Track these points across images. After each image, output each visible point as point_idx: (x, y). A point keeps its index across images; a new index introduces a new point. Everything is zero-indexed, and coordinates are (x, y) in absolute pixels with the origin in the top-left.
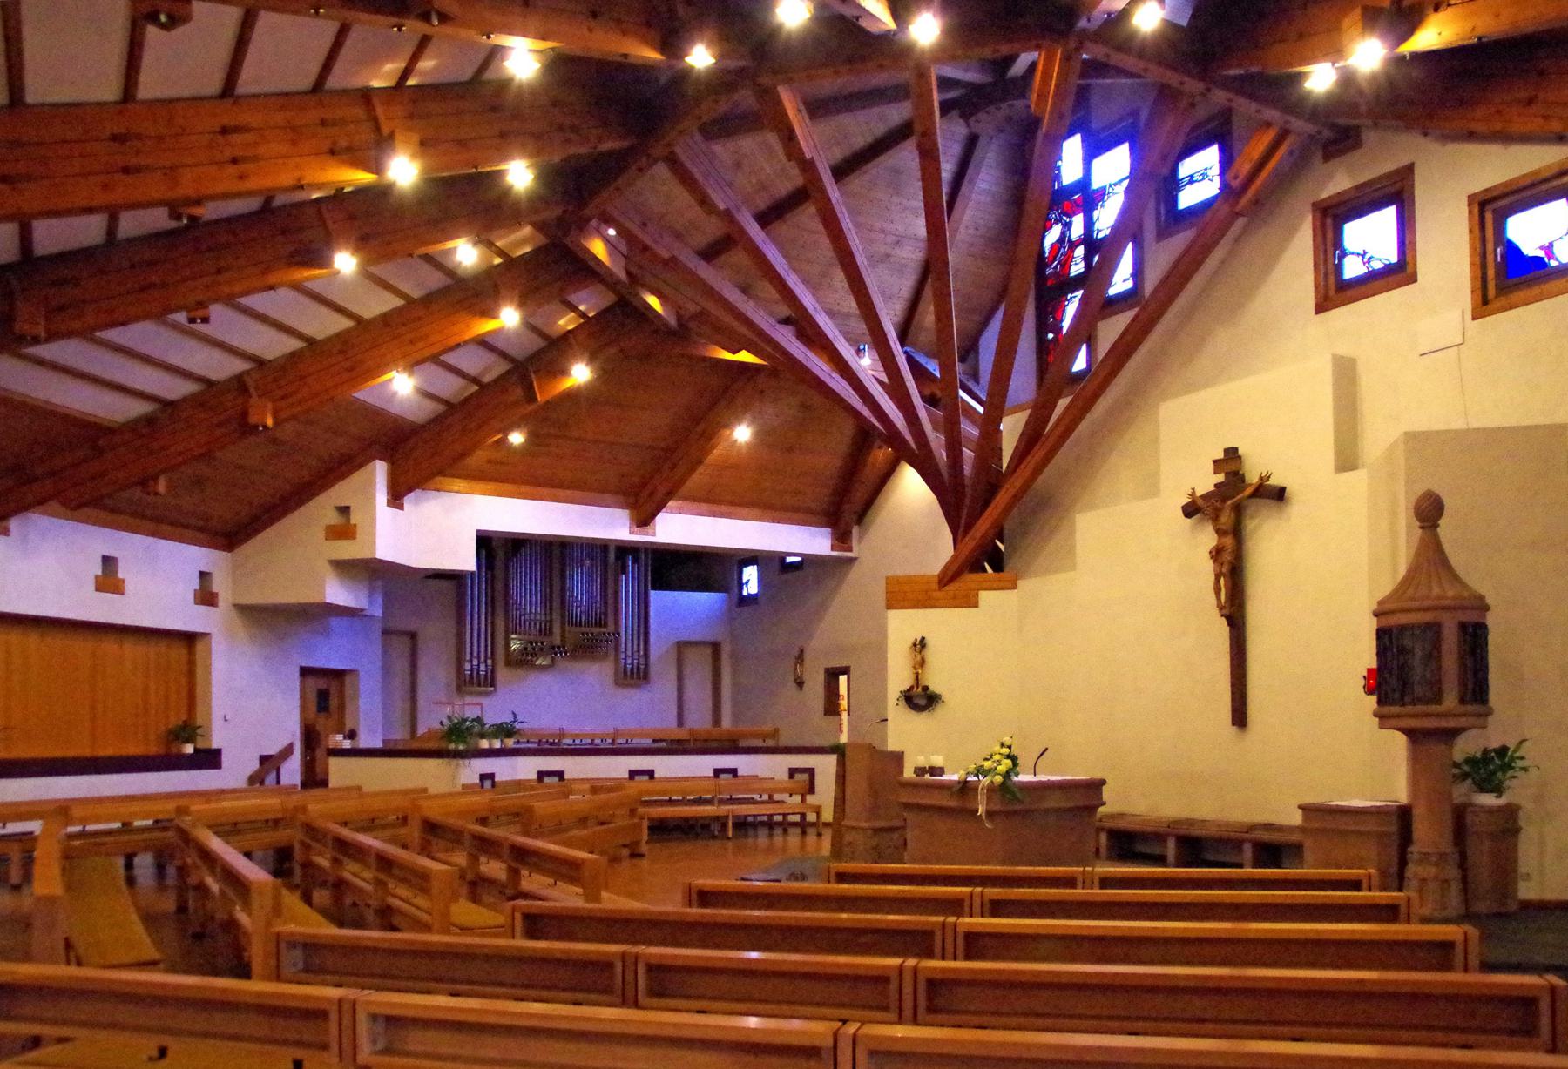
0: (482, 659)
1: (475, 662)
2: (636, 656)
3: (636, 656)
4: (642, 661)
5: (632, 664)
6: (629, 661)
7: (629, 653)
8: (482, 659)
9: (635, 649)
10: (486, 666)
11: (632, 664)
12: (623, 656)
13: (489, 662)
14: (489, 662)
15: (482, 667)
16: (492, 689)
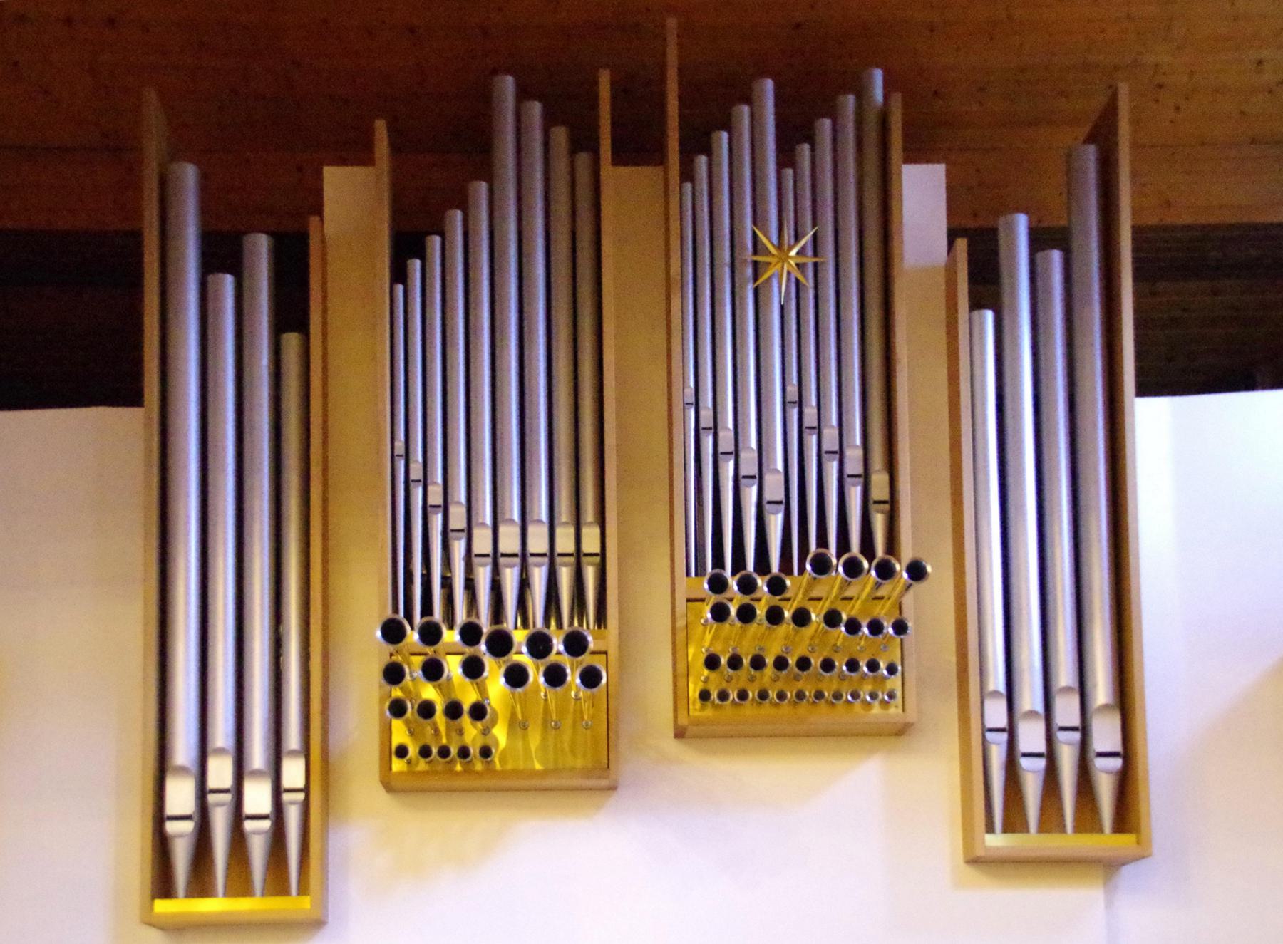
0: (258, 755)
1: (220, 772)
2: (1067, 711)
3: (1067, 711)
4: (1106, 735)
5: (1051, 756)
6: (1031, 737)
7: (1031, 697)
8: (258, 755)
9: (1065, 674)
10: (277, 791)
11: (1051, 756)
12: (996, 714)
13: (293, 773)
14: (293, 773)
15: (258, 797)
16: (306, 903)
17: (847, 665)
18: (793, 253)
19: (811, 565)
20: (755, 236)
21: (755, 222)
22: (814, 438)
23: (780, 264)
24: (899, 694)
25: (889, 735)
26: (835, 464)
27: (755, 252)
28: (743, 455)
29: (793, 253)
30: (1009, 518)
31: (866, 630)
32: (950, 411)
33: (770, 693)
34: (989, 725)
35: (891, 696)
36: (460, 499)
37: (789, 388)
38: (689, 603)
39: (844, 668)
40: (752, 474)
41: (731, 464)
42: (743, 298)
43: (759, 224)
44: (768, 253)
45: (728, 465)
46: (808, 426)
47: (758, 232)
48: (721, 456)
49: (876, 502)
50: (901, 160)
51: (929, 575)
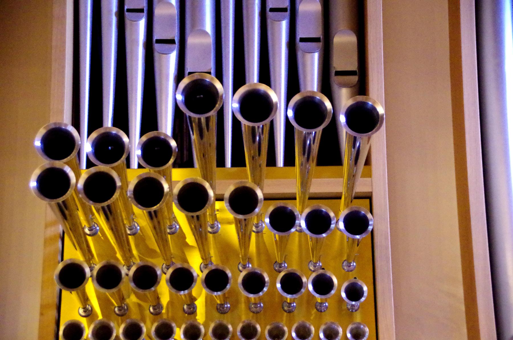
17: (283, 282)
49: (339, 73)
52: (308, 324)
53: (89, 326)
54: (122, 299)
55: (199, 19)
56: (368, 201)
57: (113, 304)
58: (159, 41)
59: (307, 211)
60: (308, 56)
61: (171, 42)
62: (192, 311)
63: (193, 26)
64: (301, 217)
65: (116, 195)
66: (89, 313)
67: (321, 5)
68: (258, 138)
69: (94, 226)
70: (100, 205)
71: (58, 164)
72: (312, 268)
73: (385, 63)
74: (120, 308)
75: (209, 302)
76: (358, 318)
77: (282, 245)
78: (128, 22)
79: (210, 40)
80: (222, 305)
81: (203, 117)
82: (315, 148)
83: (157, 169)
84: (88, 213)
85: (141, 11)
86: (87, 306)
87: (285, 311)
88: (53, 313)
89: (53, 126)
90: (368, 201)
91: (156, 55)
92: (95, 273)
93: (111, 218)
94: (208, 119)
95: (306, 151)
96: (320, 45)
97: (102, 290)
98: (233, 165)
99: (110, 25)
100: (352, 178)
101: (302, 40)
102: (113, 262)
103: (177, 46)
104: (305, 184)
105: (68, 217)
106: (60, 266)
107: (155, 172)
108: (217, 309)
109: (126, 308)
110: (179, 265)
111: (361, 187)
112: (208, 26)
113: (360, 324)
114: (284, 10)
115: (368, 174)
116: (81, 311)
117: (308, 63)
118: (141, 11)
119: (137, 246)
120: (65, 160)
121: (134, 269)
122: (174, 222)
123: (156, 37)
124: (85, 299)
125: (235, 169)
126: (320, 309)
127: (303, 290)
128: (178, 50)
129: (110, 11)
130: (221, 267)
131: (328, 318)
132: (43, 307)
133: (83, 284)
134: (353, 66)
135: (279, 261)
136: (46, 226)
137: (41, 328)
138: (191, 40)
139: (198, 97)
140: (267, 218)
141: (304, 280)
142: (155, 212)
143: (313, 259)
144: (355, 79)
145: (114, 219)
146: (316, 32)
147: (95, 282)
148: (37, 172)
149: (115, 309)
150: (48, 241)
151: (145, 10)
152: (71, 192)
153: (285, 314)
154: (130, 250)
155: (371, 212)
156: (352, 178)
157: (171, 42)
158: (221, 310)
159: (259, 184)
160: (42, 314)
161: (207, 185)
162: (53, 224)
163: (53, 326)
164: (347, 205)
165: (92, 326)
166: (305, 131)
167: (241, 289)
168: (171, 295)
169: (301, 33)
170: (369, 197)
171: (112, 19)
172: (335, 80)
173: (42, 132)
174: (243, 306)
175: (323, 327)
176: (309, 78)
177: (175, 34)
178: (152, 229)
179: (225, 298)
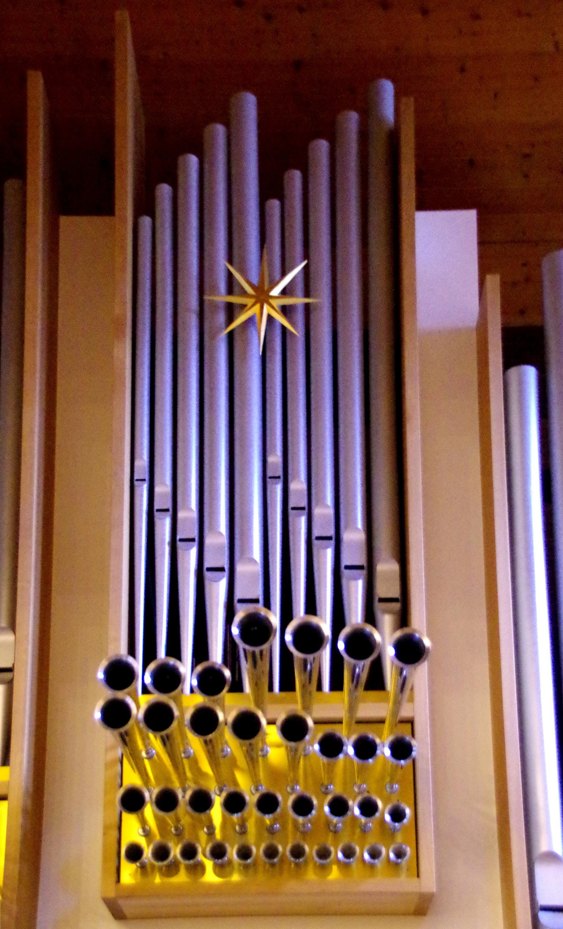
17: (331, 805)
18: (276, 291)
19: (238, 627)
20: (230, 276)
21: (230, 260)
22: (303, 520)
23: (258, 306)
24: (409, 851)
25: (405, 914)
26: (329, 553)
27: (230, 291)
28: (209, 541)
29: (276, 291)
30: (537, 397)
31: (350, 750)
32: (484, 508)
33: (229, 849)
34: (543, 899)
35: (400, 854)
36: (149, 762)
37: (271, 459)
38: (8, 665)
39: (327, 809)
40: (165, 507)
41: (193, 552)
42: (214, 350)
43: (236, 260)
44: (244, 293)
45: (189, 554)
46: (295, 506)
47: (237, 275)
48: (156, 514)
49: (382, 600)
50: (414, 204)
51: (428, 652)
52: (353, 844)
53: (148, 846)
54: (178, 820)
55: (247, 546)
56: (409, 726)
57: (169, 825)
58: (210, 569)
59: (354, 737)
60: (353, 583)
61: (222, 569)
62: (243, 831)
63: (242, 552)
64: (348, 742)
65: (175, 724)
66: (147, 834)
67: (365, 534)
68: (309, 667)
69: (151, 749)
70: (159, 734)
71: (120, 695)
72: (356, 789)
73: (428, 590)
74: (177, 829)
75: (260, 823)
76: (399, 838)
77: (330, 770)
78: (180, 552)
79: (258, 568)
80: (272, 826)
81: (257, 650)
82: (364, 677)
83: (212, 698)
84: (145, 739)
85: (193, 540)
86: (146, 826)
87: (331, 831)
88: (115, 833)
89: (114, 658)
90: (409, 726)
91: (207, 583)
92: (154, 797)
93: (167, 743)
94: (261, 652)
95: (355, 678)
96: (364, 572)
97: (161, 814)
98: (282, 689)
99: (163, 555)
100: (398, 704)
101: (347, 567)
102: (170, 786)
103: (226, 573)
104: (352, 709)
105: (129, 744)
106: (121, 791)
107: (209, 700)
108: (267, 829)
109: (181, 827)
110: (232, 789)
111: (405, 713)
112: (257, 553)
113: (401, 844)
114: (329, 538)
115: (411, 699)
116: (141, 831)
117: (353, 590)
118: (193, 540)
119: (191, 769)
120: (126, 690)
121: (189, 793)
122: (225, 745)
123: (207, 565)
124: (143, 822)
125: (284, 694)
126: (364, 830)
127: (349, 813)
128: (228, 578)
129: (164, 540)
130: (272, 790)
131: (372, 840)
132: (106, 828)
133: (142, 809)
134: (395, 592)
135: (326, 783)
136: (107, 750)
137: (105, 846)
138: (240, 568)
139: (252, 629)
140: (316, 744)
141: (350, 803)
142: (211, 741)
143: (358, 781)
144: (397, 606)
145: (171, 745)
146: (361, 560)
147: (154, 805)
148: (100, 704)
149: (171, 829)
150: (108, 765)
151: (197, 539)
152: (131, 722)
153: (331, 834)
154: (184, 773)
155: (413, 735)
156: (398, 704)
157: (222, 569)
158: (271, 831)
159: (310, 714)
160: (105, 834)
161: (260, 714)
162: (113, 748)
163: (115, 846)
164: (391, 732)
165: (151, 847)
166: (353, 661)
167: (291, 813)
168: (224, 817)
169: (346, 560)
170: (411, 722)
171: (165, 548)
172: (378, 607)
173: (104, 664)
174: (290, 827)
175: (367, 847)
176: (353, 604)
177: (195, 534)
178: (207, 752)
179: (275, 821)
